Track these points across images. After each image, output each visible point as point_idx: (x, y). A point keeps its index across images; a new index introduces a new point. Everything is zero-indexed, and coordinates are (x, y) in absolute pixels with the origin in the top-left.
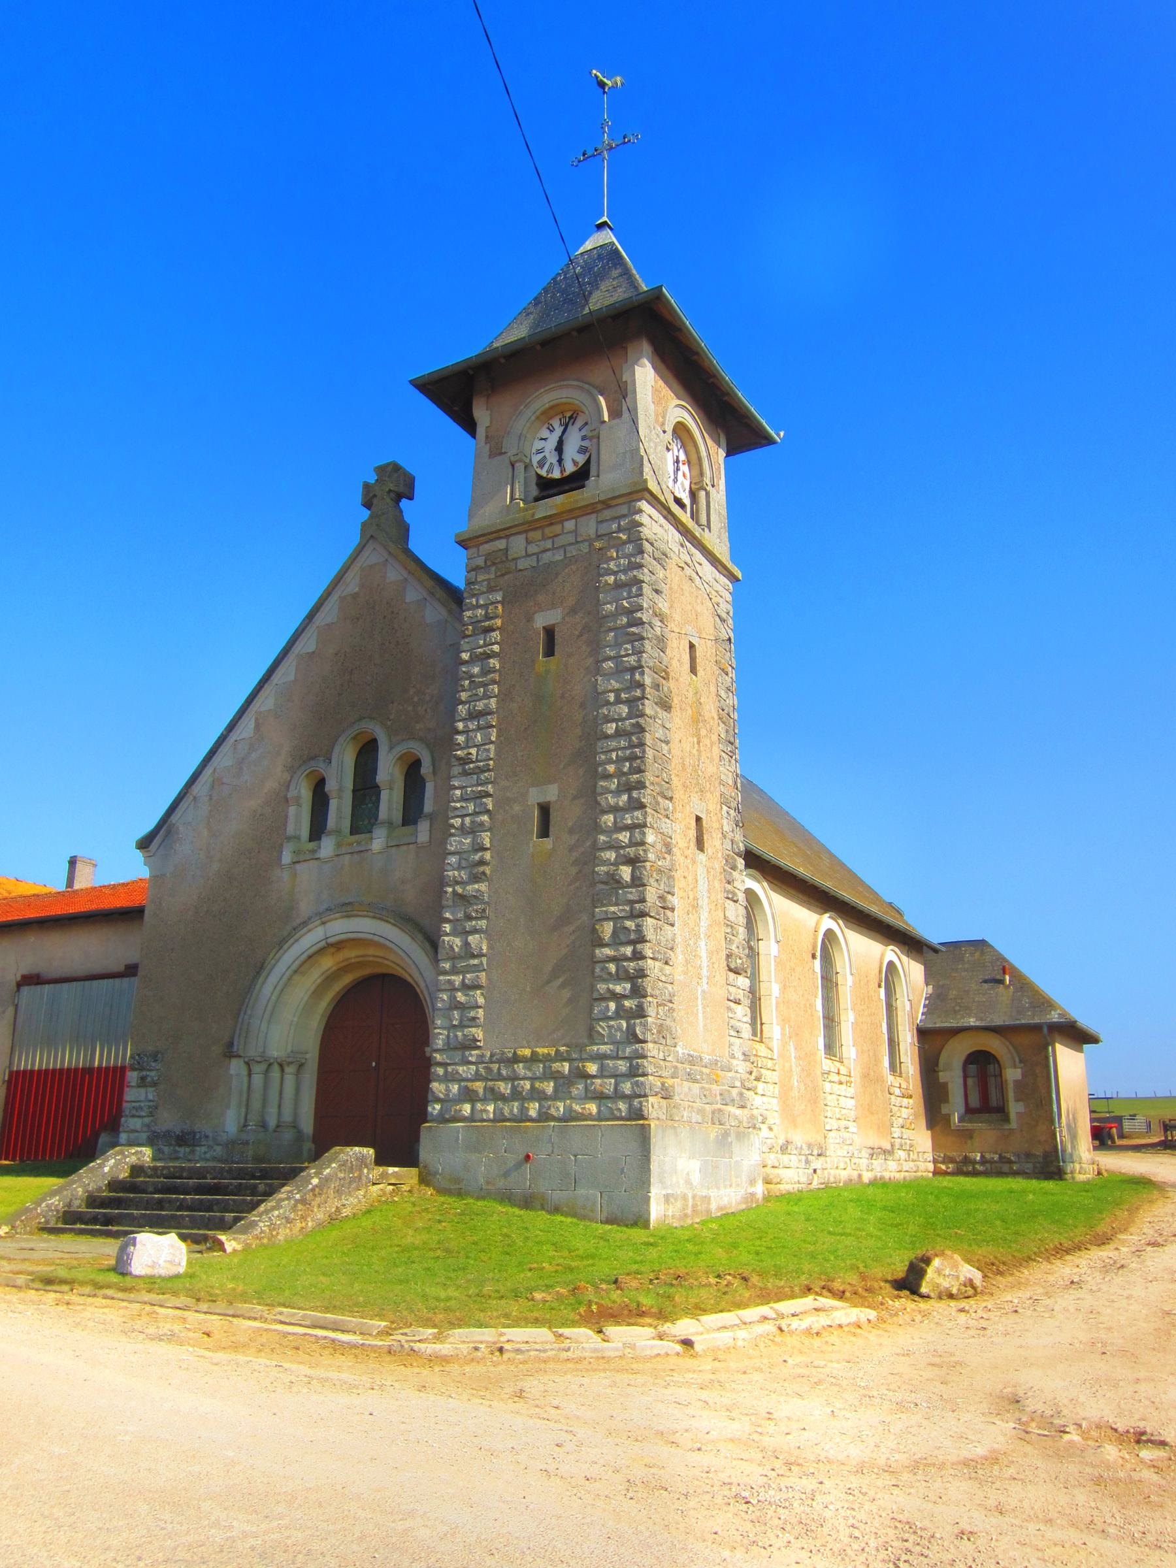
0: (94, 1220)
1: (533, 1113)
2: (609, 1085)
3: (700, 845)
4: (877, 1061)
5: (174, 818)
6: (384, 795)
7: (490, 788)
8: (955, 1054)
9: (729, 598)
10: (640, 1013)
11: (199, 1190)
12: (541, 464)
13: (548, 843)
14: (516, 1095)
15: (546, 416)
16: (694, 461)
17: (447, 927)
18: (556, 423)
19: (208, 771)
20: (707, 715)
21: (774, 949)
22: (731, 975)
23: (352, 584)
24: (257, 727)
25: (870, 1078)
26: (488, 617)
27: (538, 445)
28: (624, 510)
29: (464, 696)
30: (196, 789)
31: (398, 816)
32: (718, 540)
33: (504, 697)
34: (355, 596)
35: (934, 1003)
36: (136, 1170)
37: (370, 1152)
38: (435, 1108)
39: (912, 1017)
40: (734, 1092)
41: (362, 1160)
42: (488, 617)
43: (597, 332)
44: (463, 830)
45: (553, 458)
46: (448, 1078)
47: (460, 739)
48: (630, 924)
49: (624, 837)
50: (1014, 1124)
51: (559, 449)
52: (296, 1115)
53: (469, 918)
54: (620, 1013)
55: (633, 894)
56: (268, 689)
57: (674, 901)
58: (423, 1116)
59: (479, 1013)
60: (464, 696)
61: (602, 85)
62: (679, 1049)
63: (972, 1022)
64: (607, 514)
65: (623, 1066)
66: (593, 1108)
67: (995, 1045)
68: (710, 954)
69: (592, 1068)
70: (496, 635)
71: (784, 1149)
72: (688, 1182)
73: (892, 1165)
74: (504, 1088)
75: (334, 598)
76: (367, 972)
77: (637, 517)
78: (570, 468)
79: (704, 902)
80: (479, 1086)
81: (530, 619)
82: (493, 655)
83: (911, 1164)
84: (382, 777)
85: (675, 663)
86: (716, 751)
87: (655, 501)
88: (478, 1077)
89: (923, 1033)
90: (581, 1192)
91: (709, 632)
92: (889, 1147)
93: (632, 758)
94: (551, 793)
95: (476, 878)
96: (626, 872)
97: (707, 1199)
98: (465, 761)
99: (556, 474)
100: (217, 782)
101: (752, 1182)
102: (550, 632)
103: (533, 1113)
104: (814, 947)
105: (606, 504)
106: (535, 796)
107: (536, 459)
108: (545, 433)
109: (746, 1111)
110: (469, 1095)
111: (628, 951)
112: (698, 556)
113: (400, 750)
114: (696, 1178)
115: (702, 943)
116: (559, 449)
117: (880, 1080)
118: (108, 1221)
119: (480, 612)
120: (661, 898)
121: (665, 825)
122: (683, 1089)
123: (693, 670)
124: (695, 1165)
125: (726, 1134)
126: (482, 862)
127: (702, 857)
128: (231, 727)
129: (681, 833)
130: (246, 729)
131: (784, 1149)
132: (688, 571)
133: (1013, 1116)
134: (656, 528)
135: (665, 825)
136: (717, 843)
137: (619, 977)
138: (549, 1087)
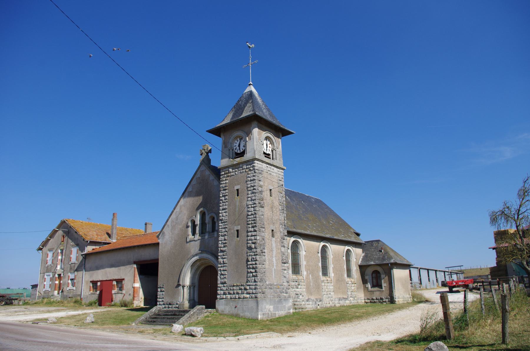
0: (151, 322)
1: (237, 297)
2: (251, 291)
3: (273, 236)
4: (342, 275)
5: (164, 230)
6: (207, 225)
7: (227, 226)
8: (369, 271)
9: (283, 174)
10: (256, 276)
11: (171, 315)
12: (236, 149)
13: (238, 239)
14: (234, 294)
15: (236, 138)
16: (272, 143)
17: (220, 257)
18: (238, 139)
19: (170, 219)
20: (275, 205)
21: (304, 253)
22: (283, 264)
23: (198, 175)
24: (180, 209)
25: (339, 280)
26: (225, 187)
27: (235, 144)
28: (251, 163)
29: (221, 205)
30: (168, 223)
31: (211, 230)
32: (279, 162)
33: (229, 205)
34: (199, 178)
35: (365, 258)
36: (159, 311)
37: (204, 306)
38: (218, 297)
39: (357, 263)
40: (284, 290)
41: (202, 308)
42: (225, 187)
43: (242, 125)
44: (222, 236)
45: (238, 148)
46: (221, 290)
47: (221, 215)
48: (254, 257)
49: (253, 238)
50: (384, 289)
51: (239, 146)
52: (194, 297)
53: (223, 255)
54: (253, 276)
55: (254, 250)
56: (190, 186)
57: (266, 251)
58: (216, 298)
59: (226, 277)
60: (221, 205)
61: (250, 47)
62: (267, 283)
63: (372, 263)
64: (248, 163)
65: (253, 287)
66: (248, 296)
67: (379, 269)
68: (276, 260)
69: (248, 287)
70: (227, 191)
71: (308, 300)
72: (269, 310)
73: (347, 302)
74: (232, 292)
75: (195, 178)
76: (207, 265)
77: (254, 164)
78: (242, 151)
79: (275, 249)
80: (227, 292)
81: (234, 187)
82: (227, 195)
83: (355, 301)
84: (207, 221)
85: (265, 196)
86: (278, 213)
87: (258, 160)
88: (227, 290)
89: (361, 267)
90: (246, 313)
91: (276, 185)
92: (346, 297)
93: (254, 220)
94: (239, 228)
95: (224, 247)
96: (253, 246)
97: (275, 314)
98: (222, 220)
99: (239, 152)
100: (172, 222)
101: (289, 309)
102: (238, 190)
103: (237, 297)
104: (318, 250)
105: (248, 161)
106: (236, 228)
107: (235, 148)
108: (236, 142)
109: (288, 294)
110: (225, 294)
111: (254, 263)
112: (273, 167)
113: (210, 215)
114: (272, 309)
115: (274, 259)
116: (239, 146)
117: (344, 280)
118: (154, 322)
119: (224, 185)
120: (261, 251)
121: (263, 234)
122: (267, 291)
123: (271, 196)
124: (272, 307)
125: (281, 300)
126: (226, 243)
127: (274, 239)
128: (171, 215)
129: (267, 234)
130: (178, 209)
131: (308, 300)
132: (269, 172)
133: (383, 287)
134: (259, 166)
135: (263, 234)
136: (279, 234)
137: (253, 268)
138: (240, 292)
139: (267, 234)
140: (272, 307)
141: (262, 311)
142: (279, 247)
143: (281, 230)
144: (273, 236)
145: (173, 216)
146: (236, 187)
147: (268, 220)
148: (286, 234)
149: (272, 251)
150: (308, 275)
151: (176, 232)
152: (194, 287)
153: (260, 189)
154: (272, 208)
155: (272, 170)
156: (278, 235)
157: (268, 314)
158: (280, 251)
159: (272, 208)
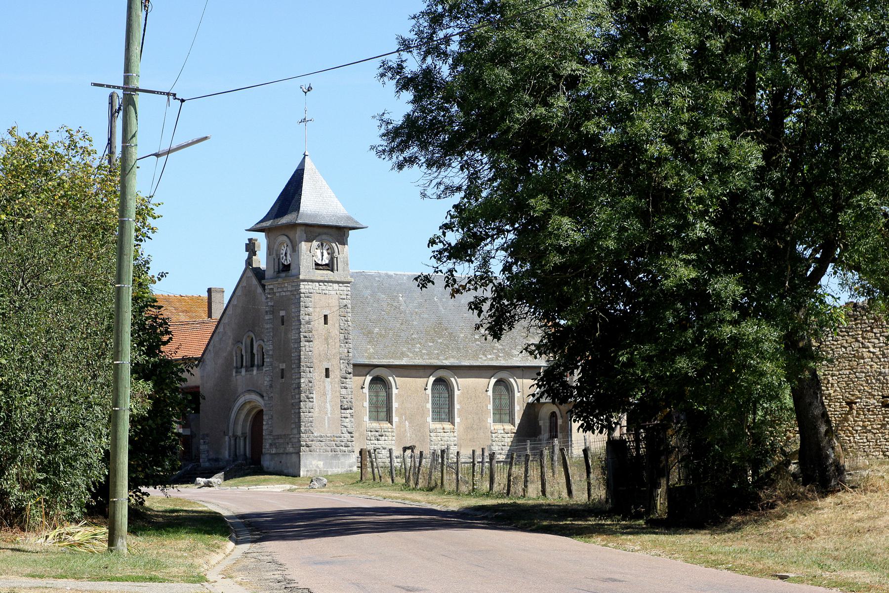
3: (327, 376)
23: (244, 284)
30: (209, 347)
31: (249, 364)
57: (314, 396)
68: (332, 406)
72: (317, 467)
84: (255, 351)
86: (338, 345)
124: (322, 463)
139: (317, 375)
140: (322, 463)
141: (305, 466)
142: (338, 389)
143: (342, 366)
144: (327, 376)
145: (216, 338)
146: (282, 313)
147: (320, 355)
148: (350, 370)
149: (325, 394)
150: (400, 422)
151: (220, 361)
152: (245, 438)
153: (307, 318)
154: (326, 339)
155: (329, 288)
156: (335, 374)
157: (316, 471)
158: (338, 394)
159: (326, 339)
